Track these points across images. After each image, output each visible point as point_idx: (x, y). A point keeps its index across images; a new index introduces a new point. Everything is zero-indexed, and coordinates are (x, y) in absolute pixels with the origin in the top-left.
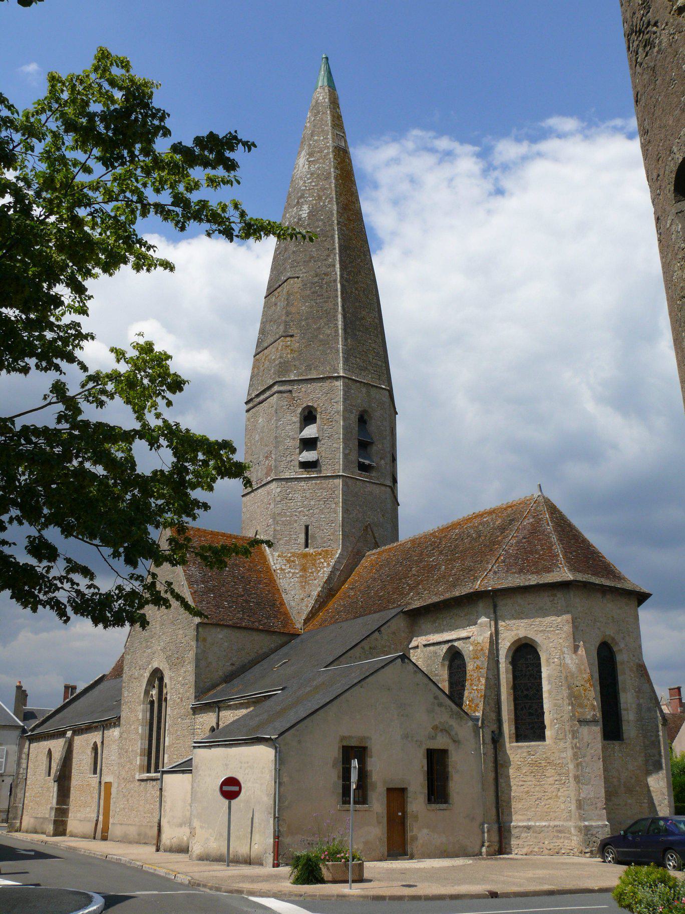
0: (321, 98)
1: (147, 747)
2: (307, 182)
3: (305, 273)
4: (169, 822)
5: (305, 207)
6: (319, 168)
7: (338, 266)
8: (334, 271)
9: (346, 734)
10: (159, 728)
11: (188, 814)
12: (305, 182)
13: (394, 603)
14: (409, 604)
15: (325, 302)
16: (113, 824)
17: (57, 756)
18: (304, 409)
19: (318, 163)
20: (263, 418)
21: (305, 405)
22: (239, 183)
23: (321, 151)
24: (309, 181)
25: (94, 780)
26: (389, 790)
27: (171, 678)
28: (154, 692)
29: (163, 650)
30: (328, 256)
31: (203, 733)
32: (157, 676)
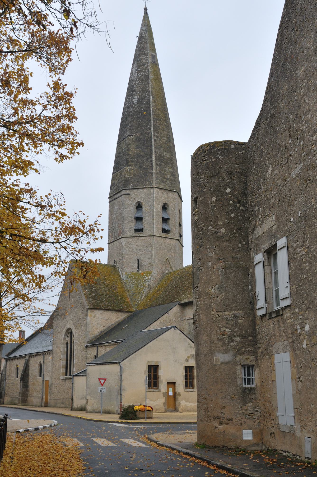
0: (144, 33)
1: (65, 364)
2: (137, 83)
3: (136, 133)
4: (76, 397)
5: (136, 97)
6: (142, 75)
7: (152, 129)
8: (151, 132)
9: (150, 360)
10: (71, 355)
11: (85, 394)
12: (136, 83)
13: (176, 299)
14: (181, 300)
15: (146, 148)
16: (50, 399)
17: (21, 369)
18: (136, 203)
19: (142, 72)
20: (117, 206)
21: (137, 201)
22: (88, 216)
23: (144, 65)
24: (138, 82)
25: (40, 379)
26: (168, 383)
27: (76, 333)
28: (68, 339)
29: (72, 320)
30: (148, 124)
31: (91, 360)
32: (70, 333)
